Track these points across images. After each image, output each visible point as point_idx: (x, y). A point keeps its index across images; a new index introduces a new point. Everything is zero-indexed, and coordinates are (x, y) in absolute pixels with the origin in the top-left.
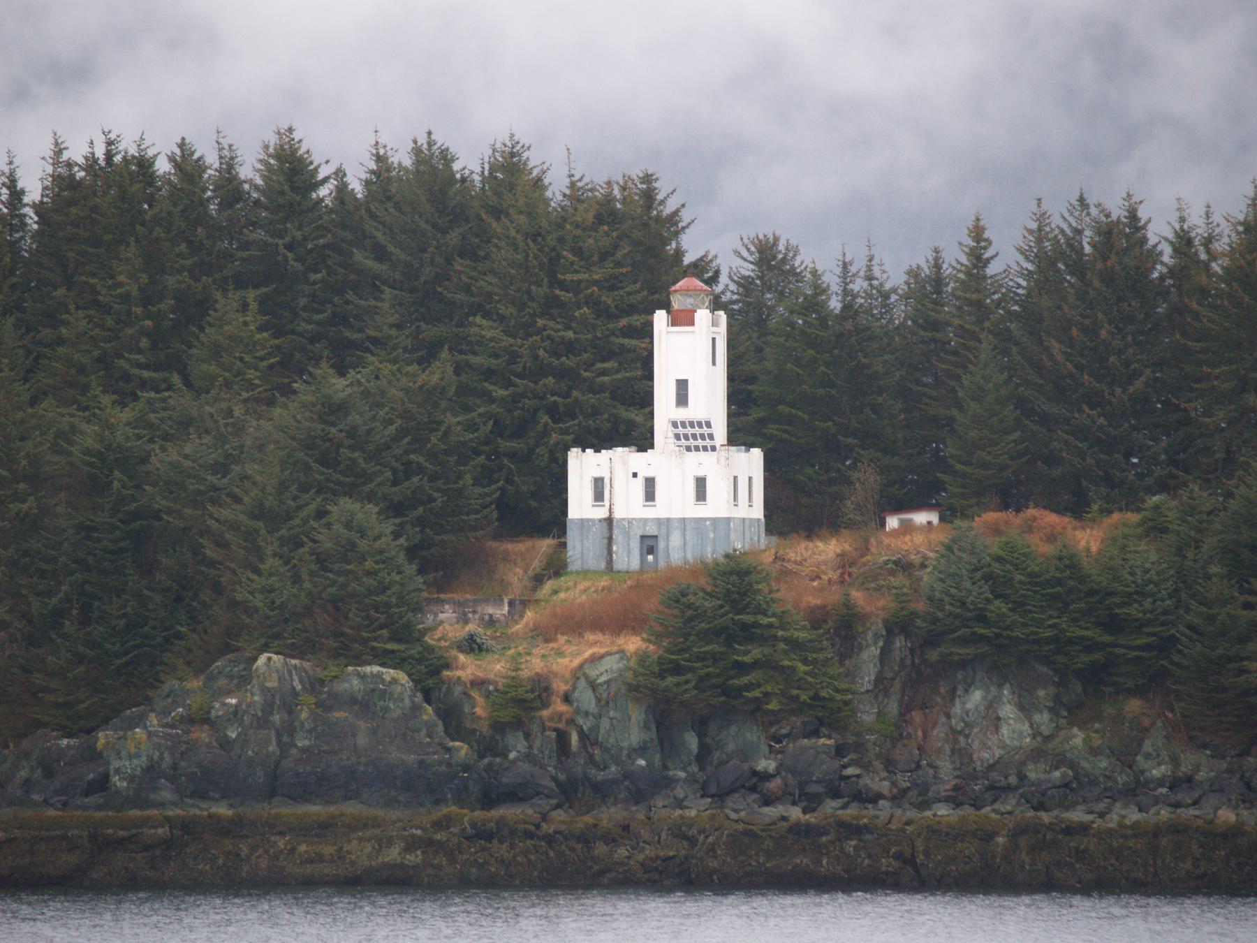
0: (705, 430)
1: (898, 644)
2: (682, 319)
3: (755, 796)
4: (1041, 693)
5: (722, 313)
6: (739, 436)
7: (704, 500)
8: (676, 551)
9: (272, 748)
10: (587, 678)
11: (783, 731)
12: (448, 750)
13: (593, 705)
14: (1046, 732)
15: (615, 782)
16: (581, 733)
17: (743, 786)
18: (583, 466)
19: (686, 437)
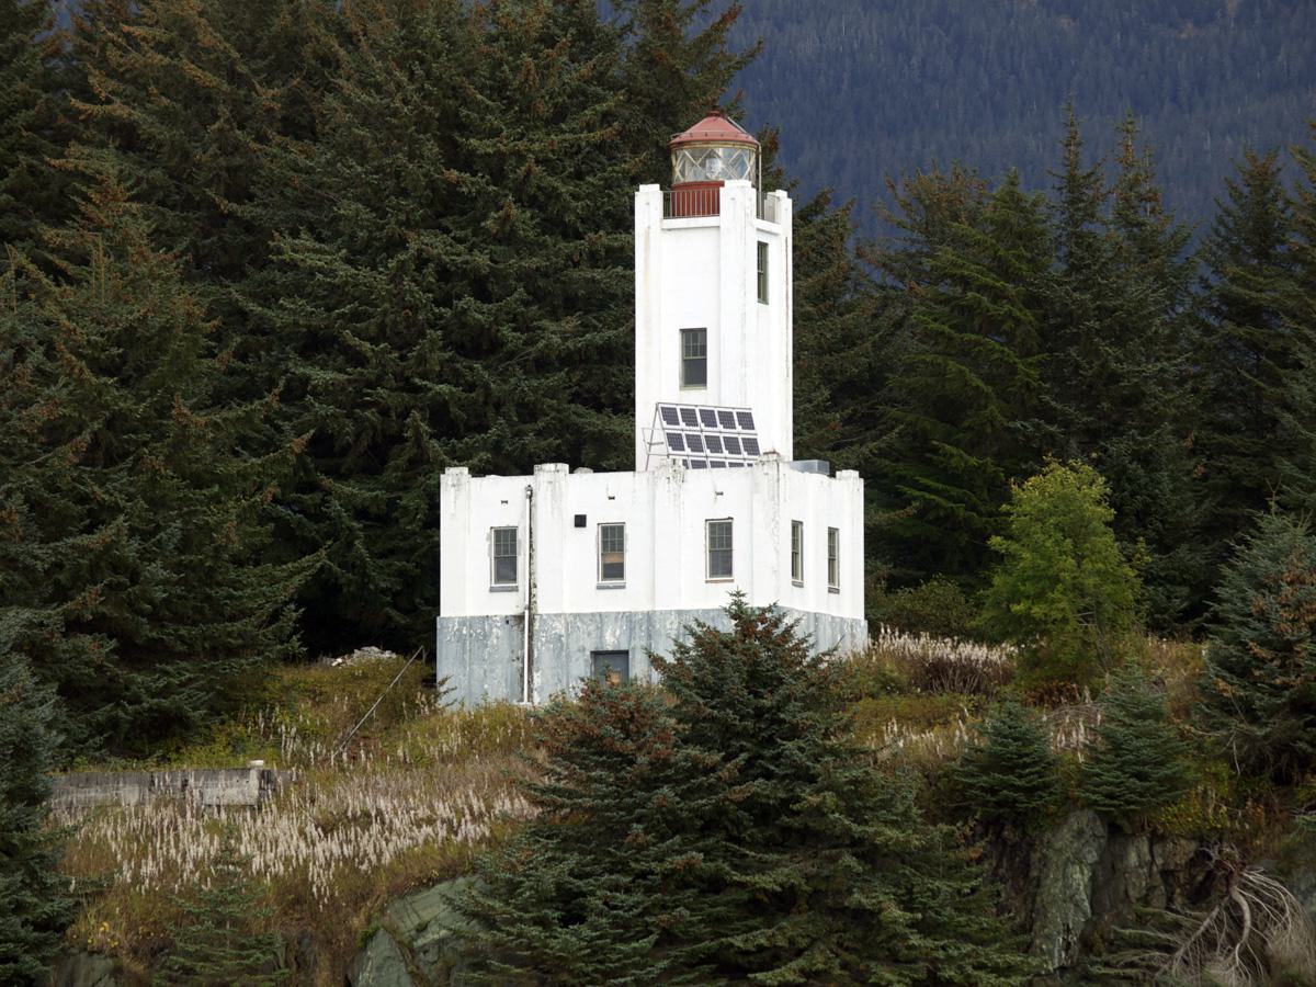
0: (739, 432)
1: (1133, 859)
5: (782, 194)
6: (818, 441)
8: (200, 753)
10: (392, 931)
18: (471, 507)
19: (695, 444)
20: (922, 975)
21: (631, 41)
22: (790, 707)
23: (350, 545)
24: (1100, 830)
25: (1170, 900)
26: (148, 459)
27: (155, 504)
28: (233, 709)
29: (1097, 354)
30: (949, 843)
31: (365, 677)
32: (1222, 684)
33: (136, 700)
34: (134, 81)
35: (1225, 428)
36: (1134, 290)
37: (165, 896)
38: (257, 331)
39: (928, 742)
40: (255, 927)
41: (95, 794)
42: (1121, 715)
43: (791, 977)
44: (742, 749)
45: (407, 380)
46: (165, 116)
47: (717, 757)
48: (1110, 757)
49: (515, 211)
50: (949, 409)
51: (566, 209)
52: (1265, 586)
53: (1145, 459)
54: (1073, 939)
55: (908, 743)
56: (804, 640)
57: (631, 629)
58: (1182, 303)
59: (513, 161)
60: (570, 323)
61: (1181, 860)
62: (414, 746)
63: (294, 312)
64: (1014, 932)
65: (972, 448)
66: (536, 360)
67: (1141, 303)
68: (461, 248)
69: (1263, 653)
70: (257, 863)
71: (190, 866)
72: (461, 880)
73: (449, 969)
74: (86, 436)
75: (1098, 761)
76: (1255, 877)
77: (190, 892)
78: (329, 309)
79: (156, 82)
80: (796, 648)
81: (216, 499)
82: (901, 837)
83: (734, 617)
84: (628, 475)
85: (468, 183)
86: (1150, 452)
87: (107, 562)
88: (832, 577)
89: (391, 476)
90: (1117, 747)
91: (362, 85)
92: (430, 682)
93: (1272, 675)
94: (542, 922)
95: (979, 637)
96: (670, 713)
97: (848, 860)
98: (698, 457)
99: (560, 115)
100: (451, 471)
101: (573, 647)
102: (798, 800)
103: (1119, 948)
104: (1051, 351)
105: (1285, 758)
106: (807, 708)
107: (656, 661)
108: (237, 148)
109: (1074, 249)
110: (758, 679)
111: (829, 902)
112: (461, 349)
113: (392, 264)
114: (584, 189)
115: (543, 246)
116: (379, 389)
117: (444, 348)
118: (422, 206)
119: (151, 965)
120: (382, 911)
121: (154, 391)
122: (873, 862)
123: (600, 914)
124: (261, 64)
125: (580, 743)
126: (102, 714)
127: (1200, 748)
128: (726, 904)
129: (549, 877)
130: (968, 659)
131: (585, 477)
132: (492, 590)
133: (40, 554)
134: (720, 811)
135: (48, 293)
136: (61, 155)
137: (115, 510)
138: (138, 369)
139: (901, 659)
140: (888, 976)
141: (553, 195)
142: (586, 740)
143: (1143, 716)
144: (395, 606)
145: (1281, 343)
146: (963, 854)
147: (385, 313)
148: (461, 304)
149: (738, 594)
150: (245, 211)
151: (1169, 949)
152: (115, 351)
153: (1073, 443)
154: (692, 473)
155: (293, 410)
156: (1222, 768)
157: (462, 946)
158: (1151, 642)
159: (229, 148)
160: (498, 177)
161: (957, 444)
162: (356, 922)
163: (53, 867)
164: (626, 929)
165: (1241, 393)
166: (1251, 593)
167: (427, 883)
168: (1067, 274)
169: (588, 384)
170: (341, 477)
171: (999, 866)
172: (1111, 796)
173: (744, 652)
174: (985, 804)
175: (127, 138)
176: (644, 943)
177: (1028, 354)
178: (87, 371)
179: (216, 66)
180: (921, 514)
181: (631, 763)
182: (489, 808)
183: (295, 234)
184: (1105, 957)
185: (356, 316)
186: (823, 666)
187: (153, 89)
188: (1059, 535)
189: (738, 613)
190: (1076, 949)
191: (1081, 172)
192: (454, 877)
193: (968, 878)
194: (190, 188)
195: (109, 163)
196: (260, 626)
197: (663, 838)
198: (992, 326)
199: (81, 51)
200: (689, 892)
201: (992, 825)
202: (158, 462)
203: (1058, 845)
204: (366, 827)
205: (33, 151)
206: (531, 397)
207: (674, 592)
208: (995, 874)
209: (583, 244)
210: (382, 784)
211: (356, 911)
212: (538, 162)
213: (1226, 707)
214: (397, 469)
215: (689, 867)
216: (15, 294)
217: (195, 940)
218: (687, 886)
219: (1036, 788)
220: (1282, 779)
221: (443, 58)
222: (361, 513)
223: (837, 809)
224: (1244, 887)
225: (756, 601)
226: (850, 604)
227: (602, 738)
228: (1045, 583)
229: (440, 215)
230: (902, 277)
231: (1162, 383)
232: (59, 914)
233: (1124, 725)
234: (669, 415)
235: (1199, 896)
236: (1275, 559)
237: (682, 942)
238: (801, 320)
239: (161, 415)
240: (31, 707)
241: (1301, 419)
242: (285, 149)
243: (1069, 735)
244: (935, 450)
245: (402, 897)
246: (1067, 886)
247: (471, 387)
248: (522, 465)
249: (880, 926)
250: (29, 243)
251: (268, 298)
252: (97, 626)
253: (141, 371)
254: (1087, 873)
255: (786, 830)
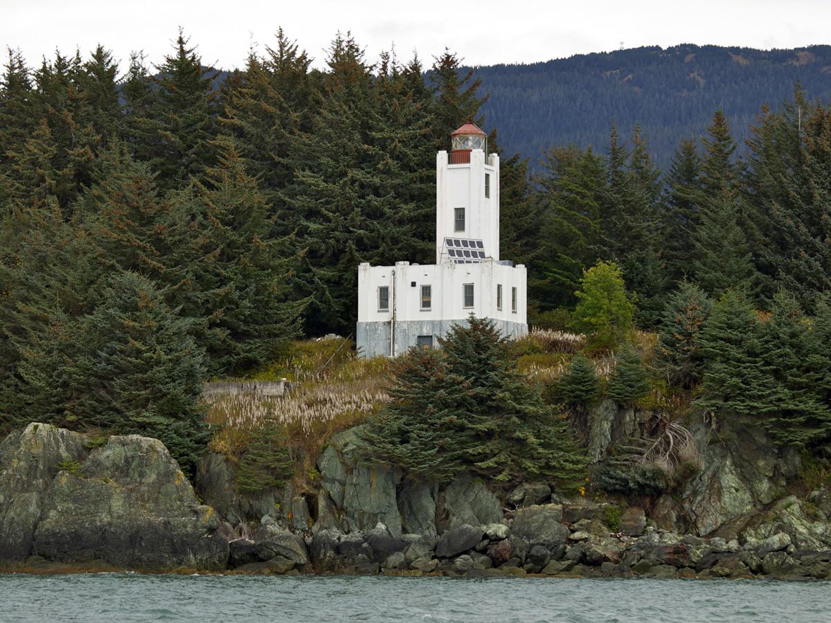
0: (477, 249)
1: (628, 418)
2: (459, 157)
3: (483, 558)
4: (761, 463)
5: (495, 155)
6: (508, 254)
7: (472, 305)
8: (261, 375)
9: (32, 509)
10: (334, 446)
11: (516, 498)
12: (196, 512)
13: (339, 472)
14: (766, 501)
15: (357, 545)
16: (329, 497)
17: (474, 549)
18: (370, 278)
19: (459, 254)
20: (543, 464)
21: (438, 94)
22: (492, 359)
23: (324, 294)
24: (615, 407)
25: (642, 435)
26: (242, 259)
27: (246, 277)
28: (277, 359)
29: (623, 219)
30: (555, 412)
31: (328, 345)
32: (664, 350)
33: (238, 354)
34: (243, 110)
35: (674, 249)
36: (638, 194)
37: (246, 431)
38: (289, 209)
39: (548, 372)
40: (281, 444)
41: (220, 391)
42: (623, 361)
43: (491, 464)
44: (473, 375)
45: (347, 228)
46: (254, 124)
47: (463, 378)
48: (619, 378)
49: (390, 161)
50: (565, 240)
51: (410, 160)
52: (681, 311)
53: (642, 261)
54: (604, 450)
55: (540, 373)
56: (498, 332)
57: (433, 327)
58: (657, 199)
59: (389, 141)
60: (412, 205)
61: (646, 419)
62: (346, 373)
63: (302, 201)
64: (581, 447)
65: (574, 256)
66: (399, 220)
67: (641, 199)
68: (369, 176)
69: (680, 337)
70: (282, 418)
71: (255, 419)
72: (361, 426)
73: (356, 461)
74: (218, 250)
75: (614, 380)
76: (675, 426)
77: (255, 430)
78: (316, 200)
79: (251, 110)
80: (495, 335)
81: (268, 275)
82: (535, 410)
83: (471, 322)
84: (432, 266)
85: (372, 150)
86: (644, 258)
87: (226, 300)
88: (514, 307)
89: (340, 266)
90: (622, 374)
91: (330, 111)
92: (354, 348)
93: (683, 346)
94: (393, 443)
95: (572, 330)
96: (444, 361)
97: (515, 419)
98: (461, 259)
99: (408, 123)
100: (362, 264)
101: (411, 334)
102: (495, 395)
103: (622, 453)
104: (605, 218)
105: (688, 379)
106: (498, 359)
107: (440, 340)
108: (283, 136)
109: (615, 177)
110: (479, 347)
111: (507, 435)
112: (369, 216)
113: (341, 182)
114: (418, 152)
115: (401, 175)
116: (336, 233)
117: (362, 215)
118: (353, 159)
119: (240, 458)
120: (330, 438)
121: (246, 232)
122: (525, 420)
123: (415, 440)
124: (292, 103)
125: (408, 372)
126: (224, 359)
127: (654, 375)
128: (466, 436)
129: (395, 425)
130: (567, 339)
131: (416, 267)
132: (378, 311)
133: (200, 296)
134: (464, 399)
135: (205, 194)
136: (214, 139)
137: (230, 279)
138: (239, 223)
139: (540, 340)
140: (529, 464)
141: (405, 155)
142: (410, 371)
143: (632, 362)
144: (341, 317)
145: (697, 215)
146: (560, 416)
147: (338, 201)
148: (369, 198)
149: (472, 313)
150: (284, 161)
151: (641, 454)
152: (231, 217)
153: (614, 254)
154: (458, 265)
155: (302, 240)
156: (663, 383)
157: (361, 452)
158: (639, 333)
159: (279, 136)
160: (384, 148)
161: (567, 255)
162: (320, 442)
163: (202, 419)
164: (426, 446)
165: (681, 235)
166: (675, 313)
167: (348, 427)
168: (612, 187)
169: (419, 230)
170: (321, 266)
171: (575, 421)
172: (619, 394)
173: (474, 337)
174: (570, 397)
175: (240, 133)
176: (433, 451)
177: (595, 219)
178: (220, 224)
179: (275, 104)
180: (552, 282)
181: (428, 380)
182: (374, 397)
183: (304, 170)
184: (616, 457)
185: (327, 203)
186: (505, 342)
187: (250, 113)
188: (602, 291)
189: (472, 321)
190: (605, 454)
191: (617, 147)
192: (358, 425)
193: (561, 426)
194: (264, 152)
195: (231, 142)
196: (287, 326)
197: (441, 410)
198: (581, 208)
199: (223, 99)
200: (451, 431)
201: (572, 405)
202: (247, 261)
203: (598, 413)
204: (325, 405)
205: (204, 138)
206: (396, 235)
207: (450, 311)
208: (573, 425)
209: (417, 174)
210: (332, 388)
211: (320, 438)
212: (399, 142)
213: (665, 359)
214: (343, 263)
215: (451, 422)
216: (192, 194)
217: (257, 448)
218: (451, 429)
219: (589, 391)
220: (687, 387)
221: (362, 101)
222: (328, 281)
223: (510, 399)
224: (671, 429)
225: (478, 317)
226: (521, 317)
227: (417, 370)
228: (596, 310)
229: (360, 163)
230: (548, 188)
231: (650, 231)
232: (205, 438)
233: (624, 366)
234: (449, 242)
235: (653, 433)
236: (685, 300)
237: (448, 451)
238: (503, 205)
239: (249, 242)
240: (194, 357)
241: (703, 245)
242: (301, 137)
243: (603, 370)
244: (559, 257)
245: (338, 432)
246: (602, 429)
247: (372, 231)
248: (391, 262)
249: (527, 445)
250: (201, 174)
251: (293, 195)
252: (222, 324)
253: (241, 224)
254: (610, 424)
255: (490, 407)
